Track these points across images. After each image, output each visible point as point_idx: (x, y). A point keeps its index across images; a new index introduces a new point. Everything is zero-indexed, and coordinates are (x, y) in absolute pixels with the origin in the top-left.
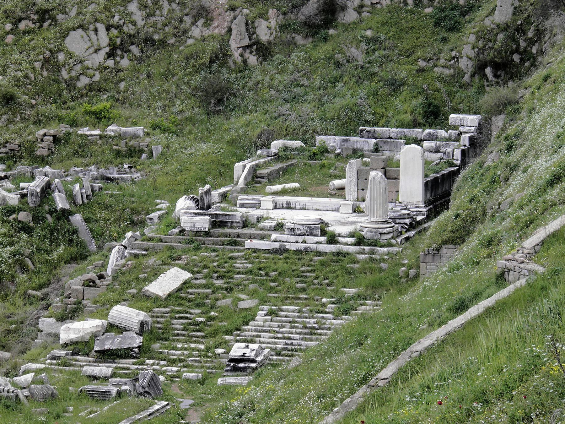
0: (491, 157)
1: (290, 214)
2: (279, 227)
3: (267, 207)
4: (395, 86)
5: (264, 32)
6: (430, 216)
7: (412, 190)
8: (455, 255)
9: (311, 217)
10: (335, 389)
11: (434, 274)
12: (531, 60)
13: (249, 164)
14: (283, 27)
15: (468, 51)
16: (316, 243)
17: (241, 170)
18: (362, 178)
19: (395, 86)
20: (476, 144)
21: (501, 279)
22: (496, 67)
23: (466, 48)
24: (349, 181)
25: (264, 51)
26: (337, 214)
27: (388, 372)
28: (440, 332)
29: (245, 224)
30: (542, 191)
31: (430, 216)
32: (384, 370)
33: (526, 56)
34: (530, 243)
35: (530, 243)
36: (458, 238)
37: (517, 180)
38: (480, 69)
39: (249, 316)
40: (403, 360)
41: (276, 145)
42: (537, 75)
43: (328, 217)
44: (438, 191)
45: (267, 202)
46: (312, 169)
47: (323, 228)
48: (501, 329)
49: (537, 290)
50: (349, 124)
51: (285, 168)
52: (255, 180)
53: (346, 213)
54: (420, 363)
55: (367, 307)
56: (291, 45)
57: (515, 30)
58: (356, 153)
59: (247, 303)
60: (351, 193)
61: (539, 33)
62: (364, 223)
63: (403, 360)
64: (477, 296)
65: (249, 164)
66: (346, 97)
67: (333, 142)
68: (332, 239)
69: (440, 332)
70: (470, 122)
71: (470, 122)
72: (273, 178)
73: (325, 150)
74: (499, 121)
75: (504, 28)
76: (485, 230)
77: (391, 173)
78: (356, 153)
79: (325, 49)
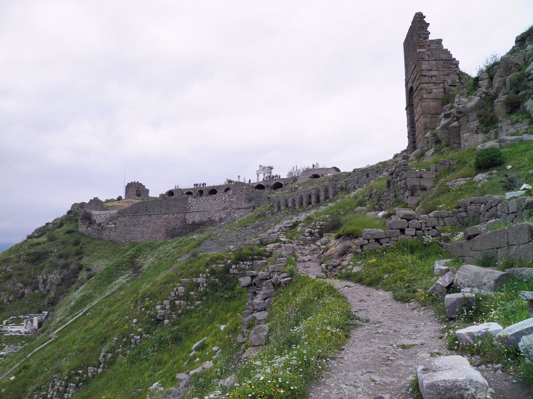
0: (49, 319)
1: (13, 329)
2: (11, 331)
3: (9, 328)
4: (33, 307)
5: (10, 299)
6: (38, 329)
7: (35, 324)
8: (42, 335)
9: (17, 329)
10: (19, 359)
11: (39, 338)
12: (57, 303)
13: (6, 321)
14: (14, 298)
15: (46, 301)
16: (18, 334)
17: (5, 322)
18: (27, 322)
19: (33, 307)
20: (47, 316)
21: (50, 339)
22: (51, 304)
23: (46, 301)
24: (24, 323)
25: (10, 302)
26: (22, 329)
27: (29, 356)
28: (39, 348)
29: (5, 331)
30: (58, 324)
31: (38, 329)
32: (210, 183)
33: (56, 302)
34: (55, 332)
35: (55, 332)
36: (43, 332)
37: (54, 322)
38: (48, 304)
39: (5, 347)
40: (32, 353)
41: (11, 317)
42: (58, 305)
43: (20, 329)
44: (40, 324)
45: (9, 327)
46: (18, 322)
47: (19, 331)
48: (49, 348)
49: (56, 340)
50: (25, 314)
51: (13, 321)
52: (7, 324)
53: (23, 329)
54: (35, 353)
55: (26, 344)
56: (15, 301)
57: (54, 298)
58: (26, 318)
59: (4, 345)
60: (25, 325)
61: (58, 298)
62: (27, 330)
63: (32, 353)
64: (46, 342)
65: (6, 321)
66: (24, 309)
67: (22, 317)
68: (21, 333)
69: (39, 348)
70: (46, 313)
71: (46, 313)
72: (10, 323)
73: (20, 318)
74: (51, 312)
75: (52, 298)
76: (48, 330)
77: (32, 321)
78: (26, 318)
79: (21, 301)
